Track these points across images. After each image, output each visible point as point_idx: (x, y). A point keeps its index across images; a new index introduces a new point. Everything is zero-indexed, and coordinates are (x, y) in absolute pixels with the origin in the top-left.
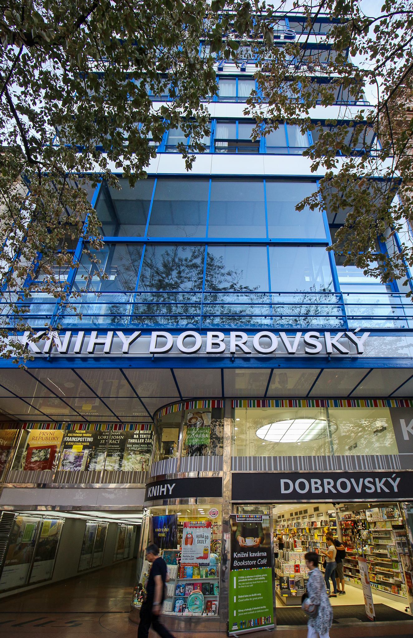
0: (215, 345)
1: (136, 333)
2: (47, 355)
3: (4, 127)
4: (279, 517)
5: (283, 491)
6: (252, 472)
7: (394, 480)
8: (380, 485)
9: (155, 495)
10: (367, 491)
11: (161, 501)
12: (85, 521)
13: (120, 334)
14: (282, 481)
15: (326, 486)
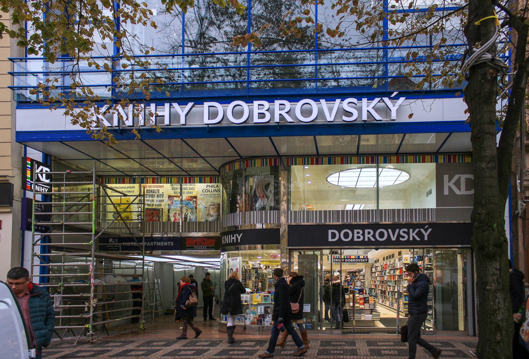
0: (262, 115)
1: (190, 104)
2: (118, 128)
3: (92, 50)
4: (376, 262)
5: (330, 240)
6: (306, 223)
7: (426, 230)
8: (413, 234)
9: (227, 242)
10: (401, 239)
11: (234, 247)
12: (171, 265)
13: (175, 105)
14: (330, 232)
15: (367, 236)
